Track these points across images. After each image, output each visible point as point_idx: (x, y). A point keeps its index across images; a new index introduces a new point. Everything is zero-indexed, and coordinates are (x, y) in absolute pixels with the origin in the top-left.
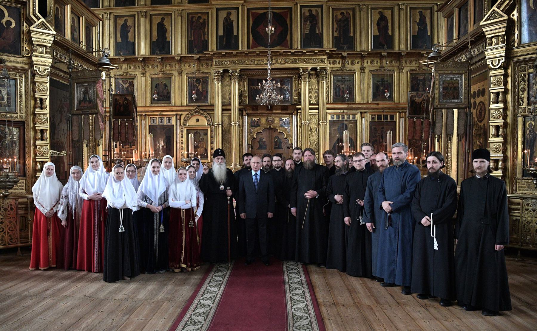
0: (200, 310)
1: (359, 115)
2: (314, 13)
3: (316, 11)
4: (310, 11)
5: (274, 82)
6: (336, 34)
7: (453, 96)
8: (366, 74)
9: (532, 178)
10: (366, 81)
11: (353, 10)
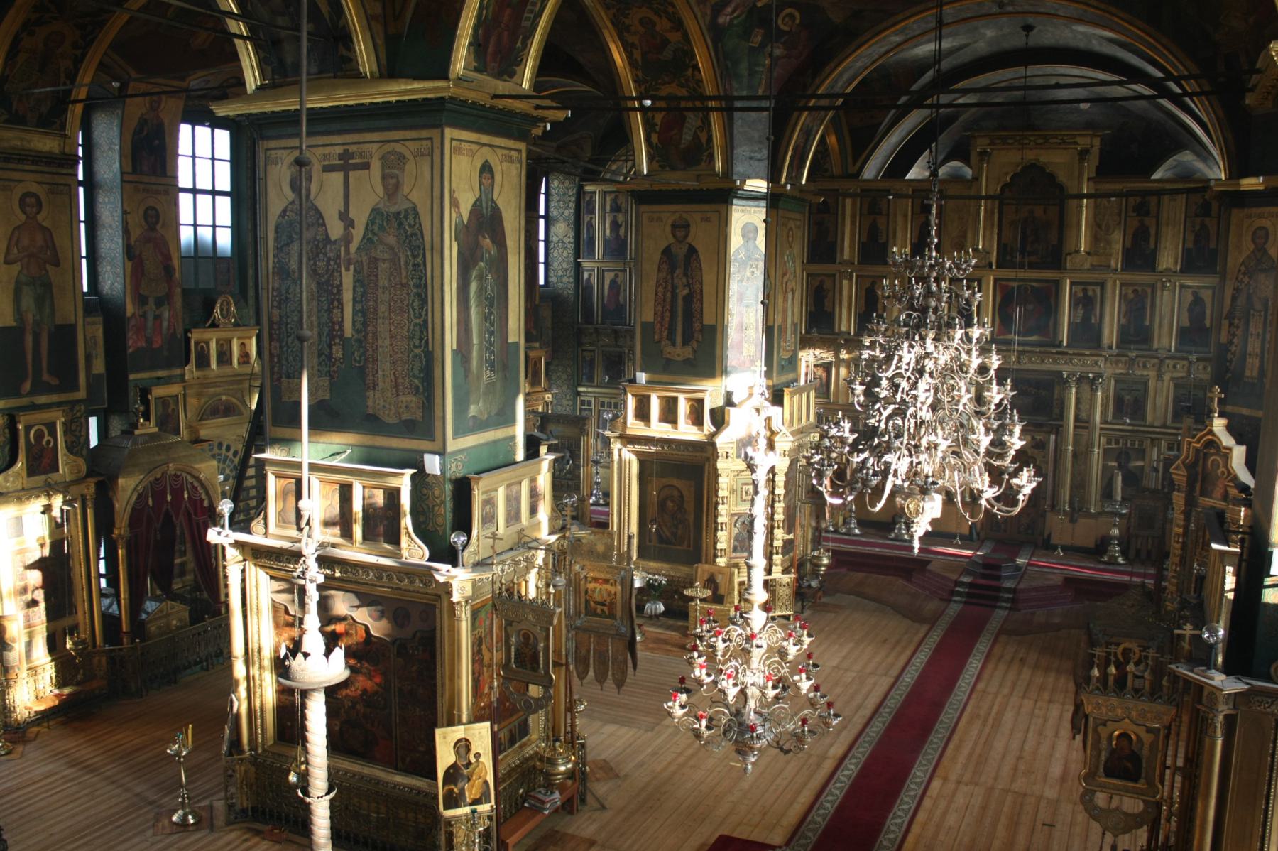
0: (912, 793)
1: (1149, 441)
2: (1090, 293)
3: (1094, 290)
4: (1085, 291)
5: (1243, 268)
6: (1123, 321)
7: (148, 401)
8: (1166, 384)
9: (224, 183)
10: (1164, 394)
11: (1153, 287)
